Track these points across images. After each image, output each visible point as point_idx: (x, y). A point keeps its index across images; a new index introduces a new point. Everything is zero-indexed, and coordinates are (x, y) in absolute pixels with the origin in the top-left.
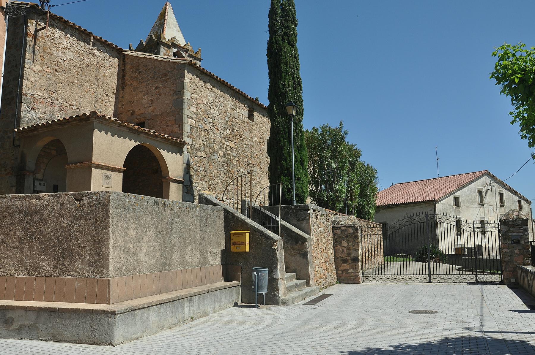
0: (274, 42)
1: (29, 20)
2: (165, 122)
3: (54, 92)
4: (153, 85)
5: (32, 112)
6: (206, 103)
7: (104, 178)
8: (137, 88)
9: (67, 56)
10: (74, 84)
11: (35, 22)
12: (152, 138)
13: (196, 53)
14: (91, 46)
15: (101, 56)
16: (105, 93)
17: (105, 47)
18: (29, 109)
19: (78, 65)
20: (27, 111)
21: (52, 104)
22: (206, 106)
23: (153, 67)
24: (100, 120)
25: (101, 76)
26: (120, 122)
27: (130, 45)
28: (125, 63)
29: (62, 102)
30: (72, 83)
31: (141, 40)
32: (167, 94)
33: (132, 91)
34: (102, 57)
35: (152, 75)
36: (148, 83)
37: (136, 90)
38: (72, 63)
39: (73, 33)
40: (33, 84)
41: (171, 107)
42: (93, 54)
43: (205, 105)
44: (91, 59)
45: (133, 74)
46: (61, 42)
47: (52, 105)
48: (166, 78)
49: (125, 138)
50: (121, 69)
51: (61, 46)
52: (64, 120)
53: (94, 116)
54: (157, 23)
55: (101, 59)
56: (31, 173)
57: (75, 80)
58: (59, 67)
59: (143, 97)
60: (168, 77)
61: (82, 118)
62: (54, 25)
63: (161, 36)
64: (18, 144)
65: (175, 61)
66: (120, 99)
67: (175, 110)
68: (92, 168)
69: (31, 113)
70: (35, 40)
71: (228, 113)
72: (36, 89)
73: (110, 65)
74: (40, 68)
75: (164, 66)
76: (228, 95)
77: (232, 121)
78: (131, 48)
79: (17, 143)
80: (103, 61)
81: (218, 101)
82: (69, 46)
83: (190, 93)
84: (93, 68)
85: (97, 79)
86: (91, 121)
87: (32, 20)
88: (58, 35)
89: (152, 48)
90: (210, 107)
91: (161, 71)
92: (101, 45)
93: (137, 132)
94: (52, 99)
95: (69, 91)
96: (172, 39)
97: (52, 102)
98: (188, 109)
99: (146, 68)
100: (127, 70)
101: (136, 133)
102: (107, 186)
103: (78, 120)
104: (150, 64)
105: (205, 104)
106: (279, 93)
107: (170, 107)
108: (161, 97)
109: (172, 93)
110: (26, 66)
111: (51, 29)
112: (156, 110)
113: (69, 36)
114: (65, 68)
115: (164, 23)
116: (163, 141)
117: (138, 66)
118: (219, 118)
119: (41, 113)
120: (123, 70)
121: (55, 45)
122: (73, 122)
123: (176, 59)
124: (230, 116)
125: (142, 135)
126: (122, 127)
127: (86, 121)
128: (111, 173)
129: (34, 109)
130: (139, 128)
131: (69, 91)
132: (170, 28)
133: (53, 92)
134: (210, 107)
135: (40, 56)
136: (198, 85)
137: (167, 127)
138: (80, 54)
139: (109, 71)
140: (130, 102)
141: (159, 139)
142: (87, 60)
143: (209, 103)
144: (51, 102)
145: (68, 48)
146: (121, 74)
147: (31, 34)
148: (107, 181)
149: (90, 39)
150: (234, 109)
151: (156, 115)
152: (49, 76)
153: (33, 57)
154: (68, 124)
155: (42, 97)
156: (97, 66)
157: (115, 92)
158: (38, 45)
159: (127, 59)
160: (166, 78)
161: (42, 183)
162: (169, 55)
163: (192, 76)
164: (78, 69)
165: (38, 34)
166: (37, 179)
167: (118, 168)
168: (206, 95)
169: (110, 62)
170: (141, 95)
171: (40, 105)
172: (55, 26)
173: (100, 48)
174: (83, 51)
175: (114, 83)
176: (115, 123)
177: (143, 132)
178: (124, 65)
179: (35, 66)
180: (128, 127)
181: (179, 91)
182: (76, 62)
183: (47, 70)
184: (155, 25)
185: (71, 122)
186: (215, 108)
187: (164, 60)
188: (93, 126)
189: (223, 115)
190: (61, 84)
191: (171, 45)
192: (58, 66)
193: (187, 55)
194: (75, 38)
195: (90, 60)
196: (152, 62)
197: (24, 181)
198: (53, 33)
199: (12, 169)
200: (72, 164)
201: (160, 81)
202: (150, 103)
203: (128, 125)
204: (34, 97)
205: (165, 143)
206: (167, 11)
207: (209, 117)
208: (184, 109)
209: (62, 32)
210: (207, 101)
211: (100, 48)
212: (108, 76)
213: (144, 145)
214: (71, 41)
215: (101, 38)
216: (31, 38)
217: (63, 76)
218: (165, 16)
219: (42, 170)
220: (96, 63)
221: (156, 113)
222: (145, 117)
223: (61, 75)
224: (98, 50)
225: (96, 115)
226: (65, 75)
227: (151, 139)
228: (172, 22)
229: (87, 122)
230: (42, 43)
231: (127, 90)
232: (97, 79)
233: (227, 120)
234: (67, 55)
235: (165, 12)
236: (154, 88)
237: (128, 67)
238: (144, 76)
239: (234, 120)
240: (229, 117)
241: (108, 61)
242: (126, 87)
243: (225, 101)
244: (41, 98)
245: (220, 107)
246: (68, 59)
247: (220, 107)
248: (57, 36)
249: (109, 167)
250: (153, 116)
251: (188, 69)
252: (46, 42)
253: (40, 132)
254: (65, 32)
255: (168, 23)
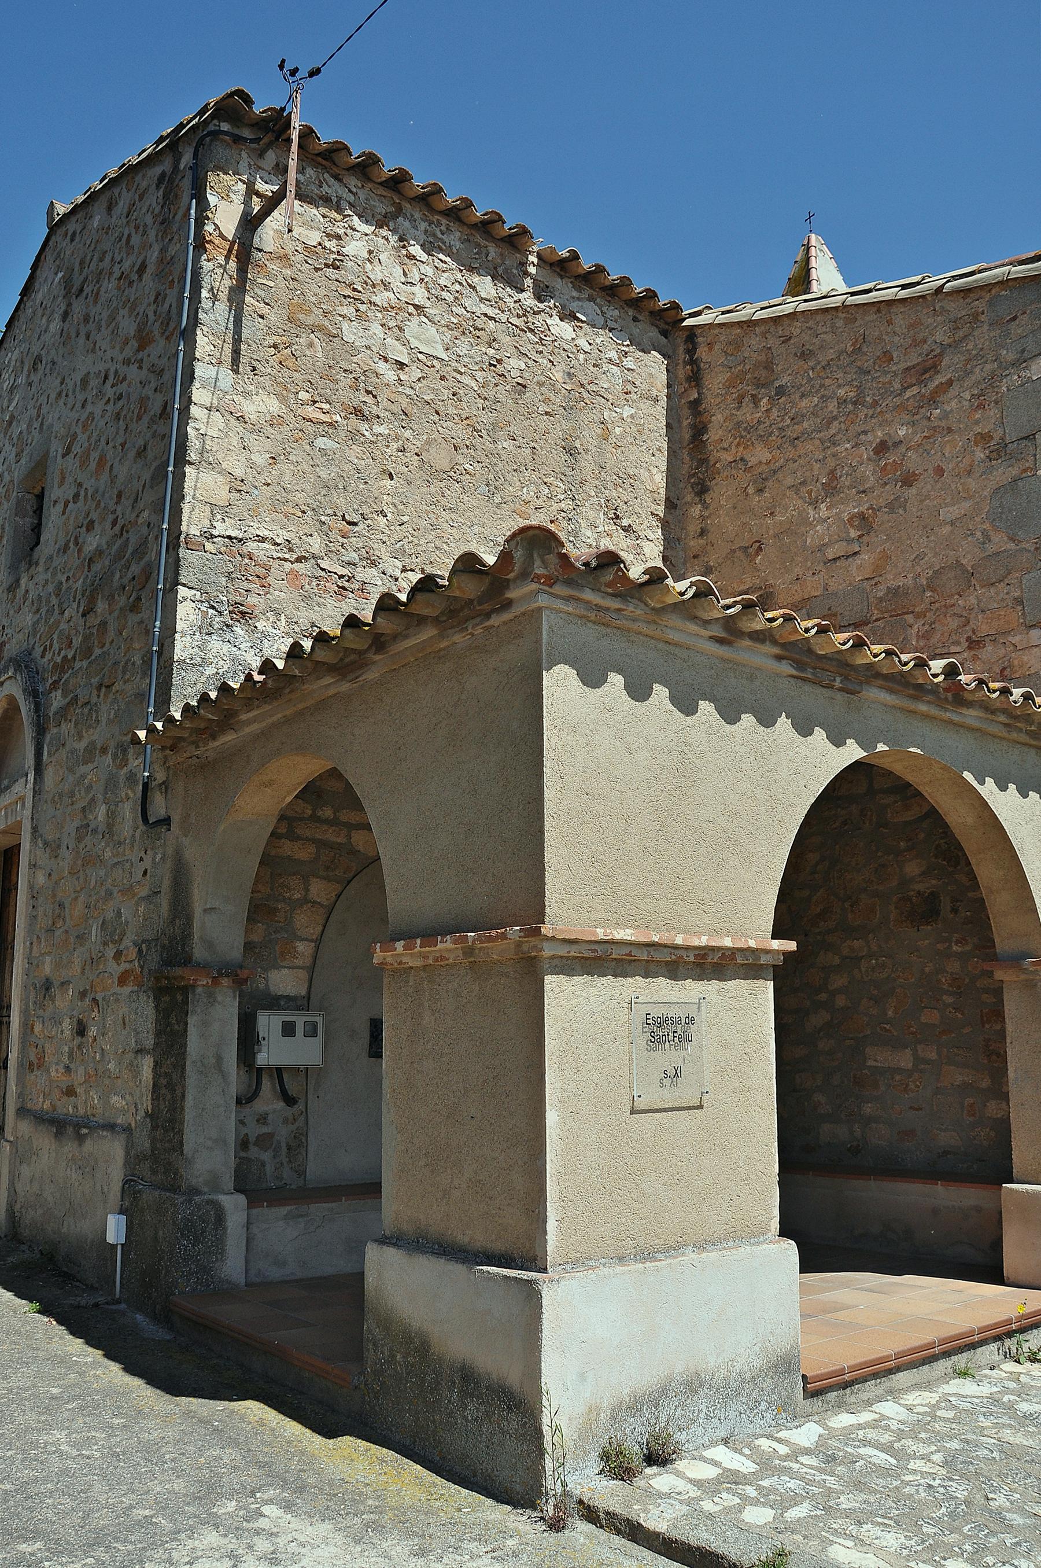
1: (211, 177)
2: (953, 623)
3: (355, 524)
5: (238, 630)
7: (642, 1040)
8: (775, 472)
9: (414, 343)
10: (456, 477)
11: (242, 187)
12: (934, 711)
14: (528, 299)
15: (582, 342)
16: (617, 517)
17: (598, 300)
18: (220, 613)
19: (473, 384)
20: (206, 629)
21: (346, 584)
24: (588, 595)
25: (588, 438)
26: (735, 603)
28: (698, 367)
29: (397, 573)
30: (452, 475)
32: (947, 467)
33: (751, 490)
34: (587, 348)
35: (847, 388)
36: (832, 431)
37: (770, 483)
38: (443, 378)
39: (434, 235)
40: (238, 486)
41: (984, 532)
42: (542, 335)
44: (534, 356)
45: (744, 410)
46: (380, 276)
47: (344, 588)
48: (932, 385)
49: (767, 720)
50: (683, 401)
51: (382, 298)
52: (348, 631)
53: (538, 563)
55: (581, 357)
56: (220, 975)
57: (460, 459)
58: (375, 397)
59: (811, 512)
61: (457, 593)
62: (339, 198)
64: (162, 813)
66: (692, 543)
67: (1011, 546)
68: (548, 979)
69: (228, 636)
70: (242, 270)
72: (255, 513)
73: (630, 387)
74: (276, 401)
79: (159, 807)
80: (594, 366)
82: (420, 296)
84: (546, 401)
85: (570, 451)
86: (516, 610)
87: (226, 173)
88: (359, 244)
91: (895, 355)
92: (575, 294)
93: (846, 678)
94: (346, 559)
95: (431, 515)
97: (341, 571)
99: (811, 364)
100: (710, 401)
101: (838, 684)
102: (667, 1097)
103: (436, 621)
104: (828, 337)
107: (979, 534)
108: (913, 491)
109: (980, 455)
110: (199, 395)
111: (324, 217)
112: (896, 566)
113: (416, 250)
114: (404, 402)
116: (994, 729)
117: (769, 366)
119: (287, 633)
120: (695, 405)
121: (348, 292)
122: (407, 637)
123: (980, 272)
125: (876, 694)
126: (747, 642)
127: (488, 616)
128: (692, 990)
129: (243, 615)
130: (859, 644)
131: (431, 515)
133: (350, 523)
135: (275, 346)
137: (970, 648)
138: (478, 333)
139: (627, 412)
140: (745, 549)
141: (971, 716)
142: (515, 364)
144: (341, 577)
145: (416, 307)
146: (685, 423)
147: (221, 236)
148: (669, 1057)
149: (523, 264)
151: (895, 592)
152: (321, 442)
153: (236, 352)
154: (377, 657)
155: (290, 550)
156: (569, 391)
157: (660, 511)
158: (263, 294)
159: (706, 349)
160: (932, 385)
161: (300, 1021)
164: (472, 407)
165: (256, 240)
166: (274, 1003)
167: (741, 950)
169: (628, 370)
170: (800, 502)
171: (281, 593)
172: (344, 204)
173: (574, 306)
174: (491, 318)
175: (654, 471)
176: (694, 618)
177: (878, 675)
178: (695, 379)
179: (246, 394)
180: (783, 646)
181: (1026, 438)
182: (461, 373)
183: (311, 412)
185: (395, 637)
187: (904, 294)
188: (538, 641)
190: (391, 477)
192: (368, 392)
194: (448, 259)
195: (530, 362)
196: (840, 323)
197: (186, 1024)
198: (338, 237)
199: (140, 951)
200: (408, 935)
201: (900, 408)
202: (853, 533)
203: (789, 626)
204: (245, 550)
205: (1002, 739)
206: (813, 263)
209: (384, 232)
211: (574, 306)
212: (623, 436)
213: (885, 763)
214: (429, 271)
215: (574, 256)
216: (221, 260)
217: (397, 438)
218: (810, 282)
219: (301, 946)
220: (558, 375)
221: (893, 584)
222: (835, 615)
223: (387, 438)
224: (568, 316)
225: (552, 558)
226: (408, 434)
227: (926, 716)
229: (495, 620)
230: (282, 284)
231: (722, 493)
232: (570, 451)
234: (412, 340)
236: (865, 453)
237: (715, 382)
238: (805, 403)
241: (617, 365)
242: (718, 479)
244: (287, 556)
246: (420, 356)
248: (355, 248)
249: (676, 947)
250: (881, 599)
252: (300, 277)
253: (248, 730)
254: (394, 231)
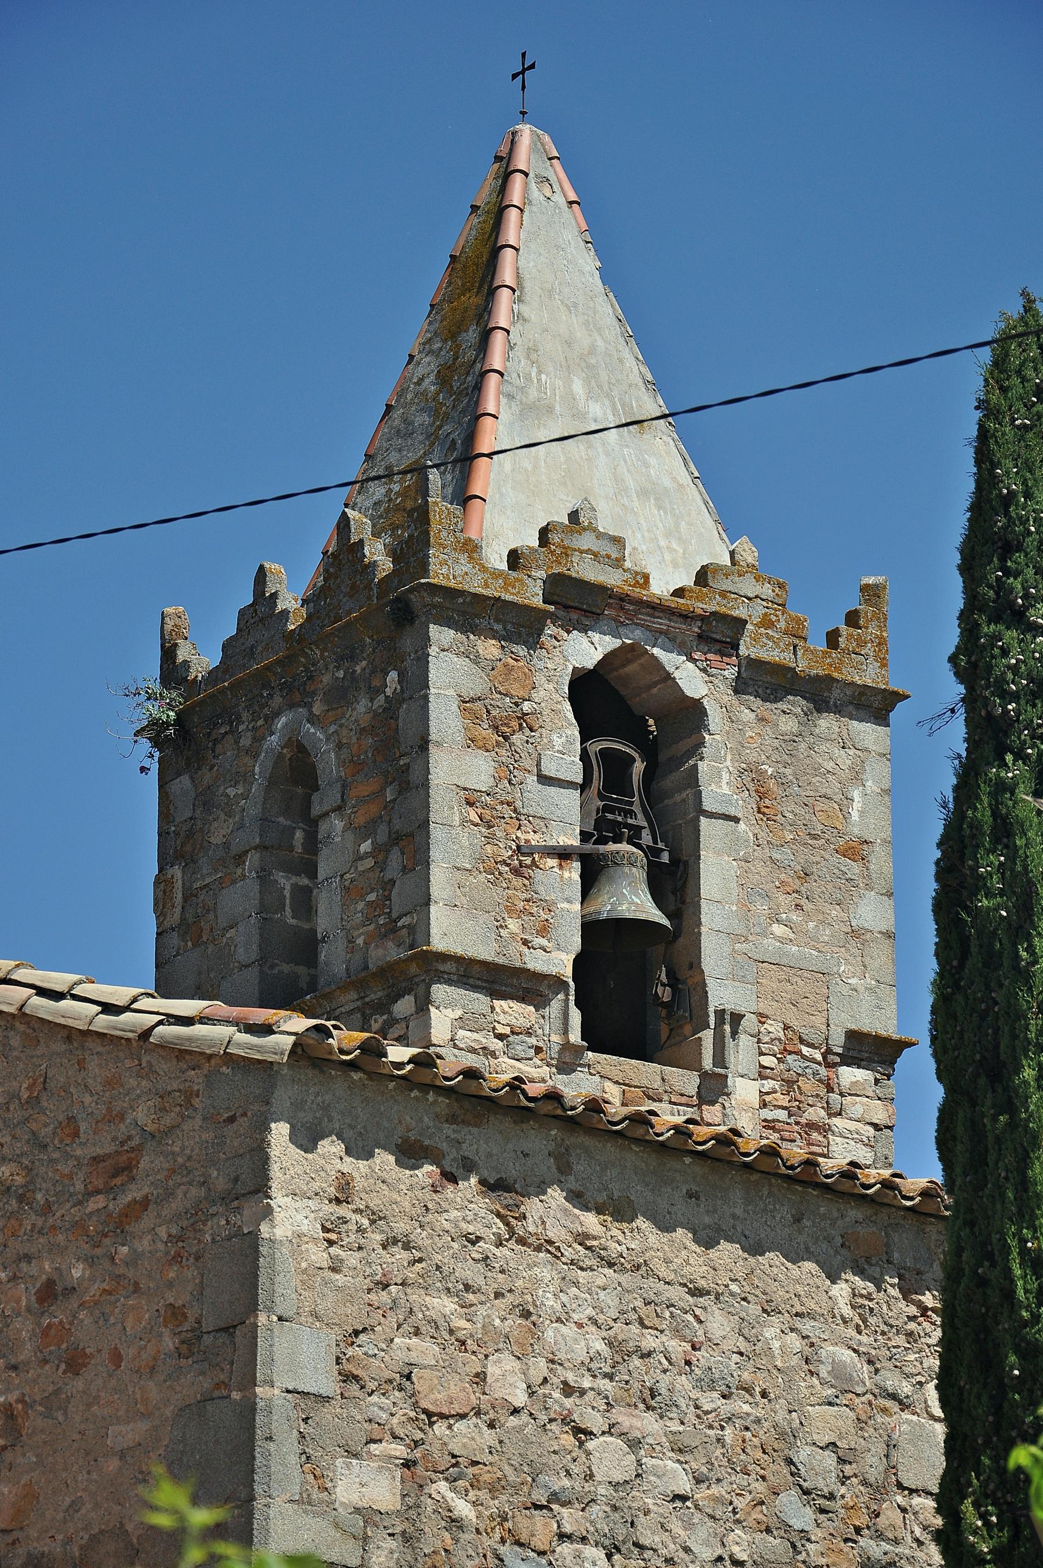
0: (987, 829)
4: (23, 1265)
6: (520, 1398)
13: (832, 638)
22: (519, 1430)
23: (25, 1095)
27: (168, 627)
31: (262, 568)
43: (513, 1421)
54: (421, 371)
60: (134, 1193)
63: (434, 527)
65: (190, 1039)
71: (803, 1454)
75: (109, 1083)
76: (809, 1266)
77: (862, 1520)
78: (180, 658)
81: (678, 1348)
83: (333, 1335)
89: (353, 658)
90: (578, 1431)
91: (83, 1127)
96: (555, 538)
98: (303, 1501)
105: (516, 1411)
106: (1013, 1358)
109: (169, 1343)
115: (484, 374)
118: (689, 1526)
124: (843, 1480)
132: (550, 410)
134: (578, 1431)
136: (420, 1237)
143: (568, 1390)
150: (894, 1397)
162: (526, 707)
163: (349, 1165)
168: (526, 1314)
184: (401, 393)
186: (647, 1424)
187: (104, 1022)
189: (741, 1479)
191: (538, 601)
193: (731, 673)
201: (78, 1226)
206: (511, 234)
207: (568, 1529)
208: (258, 1504)
210: (539, 1368)
218: (492, 292)
228: (569, 344)
233: (801, 1517)
235: (496, 251)
236: (24, 1295)
239: (890, 1516)
240: (827, 1483)
243: (769, 1333)
245: (710, 1401)
247: (710, 1401)
251: (298, 1105)
255: (519, 364)
